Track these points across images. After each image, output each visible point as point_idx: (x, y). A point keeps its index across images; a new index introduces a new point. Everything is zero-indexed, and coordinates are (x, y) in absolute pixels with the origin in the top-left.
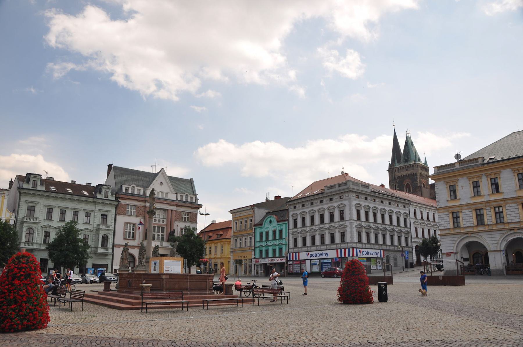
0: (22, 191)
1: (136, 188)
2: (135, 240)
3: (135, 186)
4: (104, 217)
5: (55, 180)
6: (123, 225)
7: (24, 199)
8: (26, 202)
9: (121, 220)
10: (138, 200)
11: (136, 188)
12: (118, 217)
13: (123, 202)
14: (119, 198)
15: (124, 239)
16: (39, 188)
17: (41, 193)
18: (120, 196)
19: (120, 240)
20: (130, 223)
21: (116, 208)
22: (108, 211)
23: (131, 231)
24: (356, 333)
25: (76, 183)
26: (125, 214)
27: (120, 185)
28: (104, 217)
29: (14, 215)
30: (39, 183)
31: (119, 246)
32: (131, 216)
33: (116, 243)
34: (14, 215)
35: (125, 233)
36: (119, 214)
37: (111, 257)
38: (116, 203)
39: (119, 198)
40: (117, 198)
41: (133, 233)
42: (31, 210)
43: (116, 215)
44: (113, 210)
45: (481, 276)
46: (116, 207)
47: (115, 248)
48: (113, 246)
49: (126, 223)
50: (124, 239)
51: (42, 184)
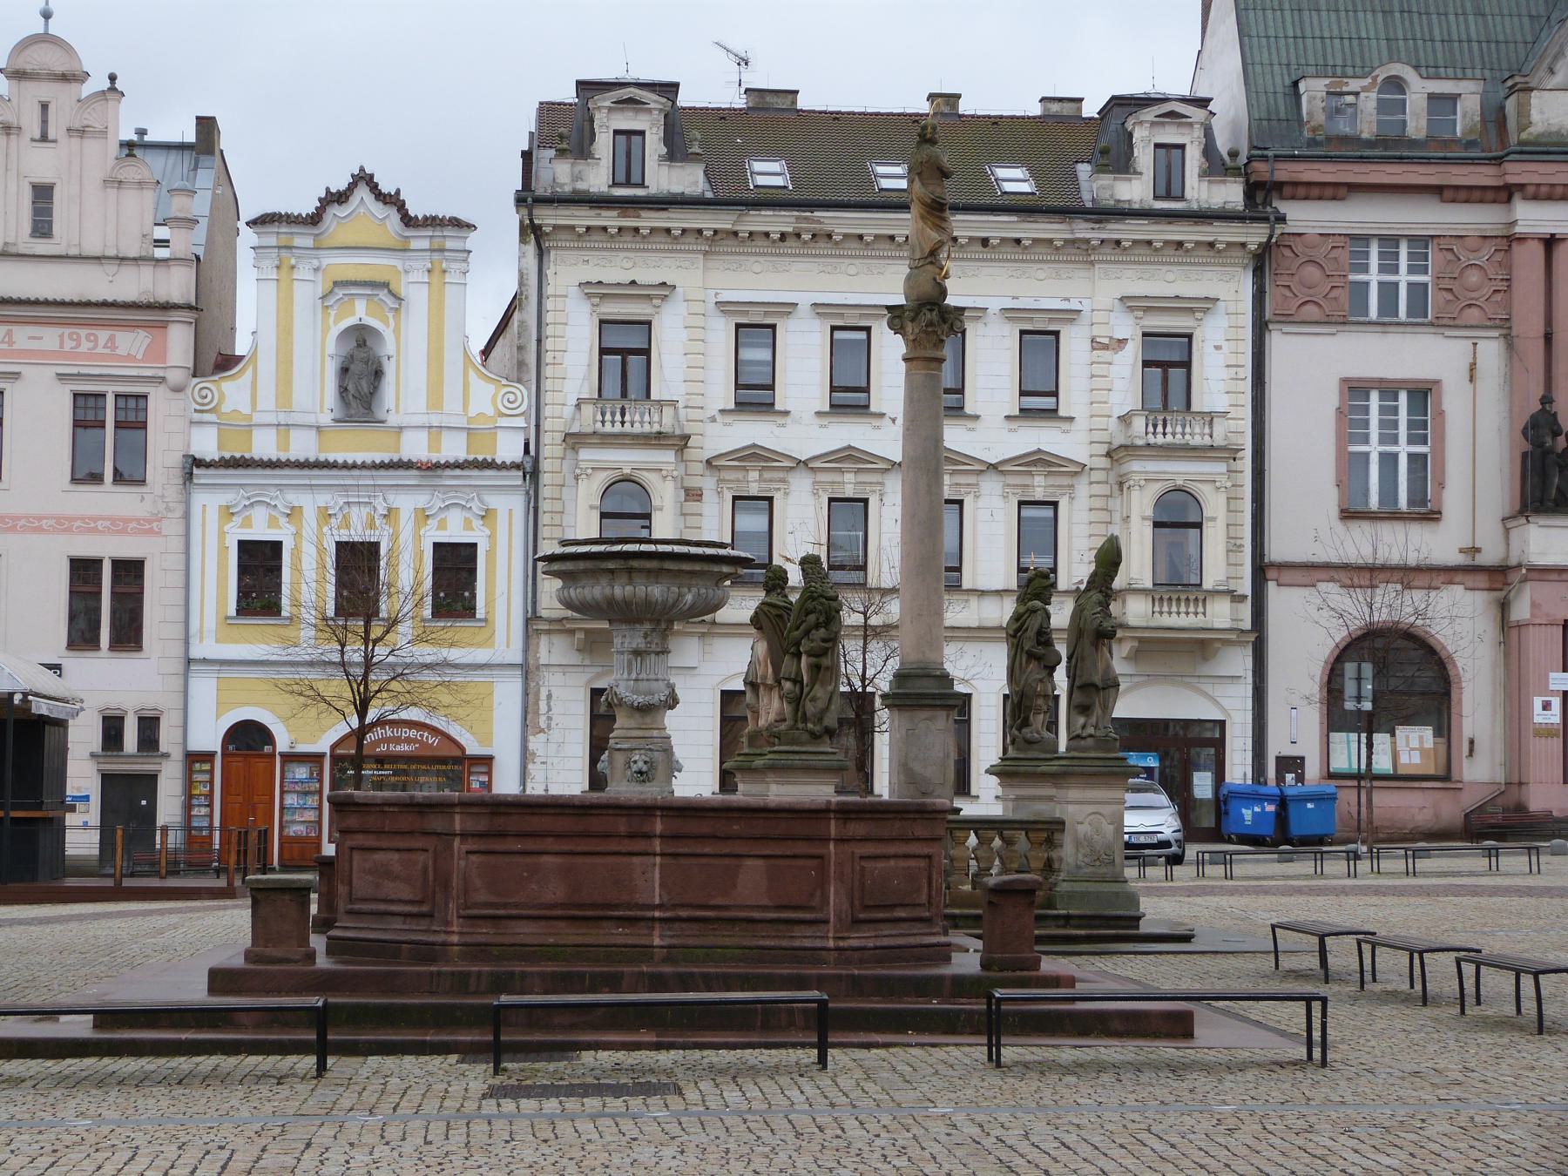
0: (548, 217)
1: (1419, 89)
2: (1432, 516)
3: (1408, 74)
4: (1168, 363)
5: (803, 103)
6: (1331, 399)
7: (569, 272)
8: (595, 291)
9: (1312, 365)
10: (1439, 192)
11: (1419, 89)
12: (1280, 344)
13: (1302, 217)
14: (1278, 188)
15: (1349, 515)
16: (662, 178)
17: (677, 220)
18: (1284, 172)
19: (1306, 523)
20: (1388, 389)
21: (1259, 272)
22: (1205, 305)
23: (1403, 449)
24: (1442, 1093)
25: (965, 107)
26: (1344, 312)
27: (1281, 81)
28: (1168, 363)
29: (522, 395)
30: (654, 145)
31: (1311, 571)
32: (1388, 321)
33: (1277, 550)
34: (522, 395)
35: (1351, 468)
36: (1287, 319)
37: (1240, 662)
38: (1255, 235)
39: (1278, 188)
40: (1262, 196)
41: (1417, 461)
42: (626, 353)
43: (1260, 328)
44: (1234, 290)
45: (1454, 695)
46: (1261, 262)
47: (1277, 597)
48: (1261, 570)
49: (1355, 390)
50: (1349, 515)
51: (676, 151)
